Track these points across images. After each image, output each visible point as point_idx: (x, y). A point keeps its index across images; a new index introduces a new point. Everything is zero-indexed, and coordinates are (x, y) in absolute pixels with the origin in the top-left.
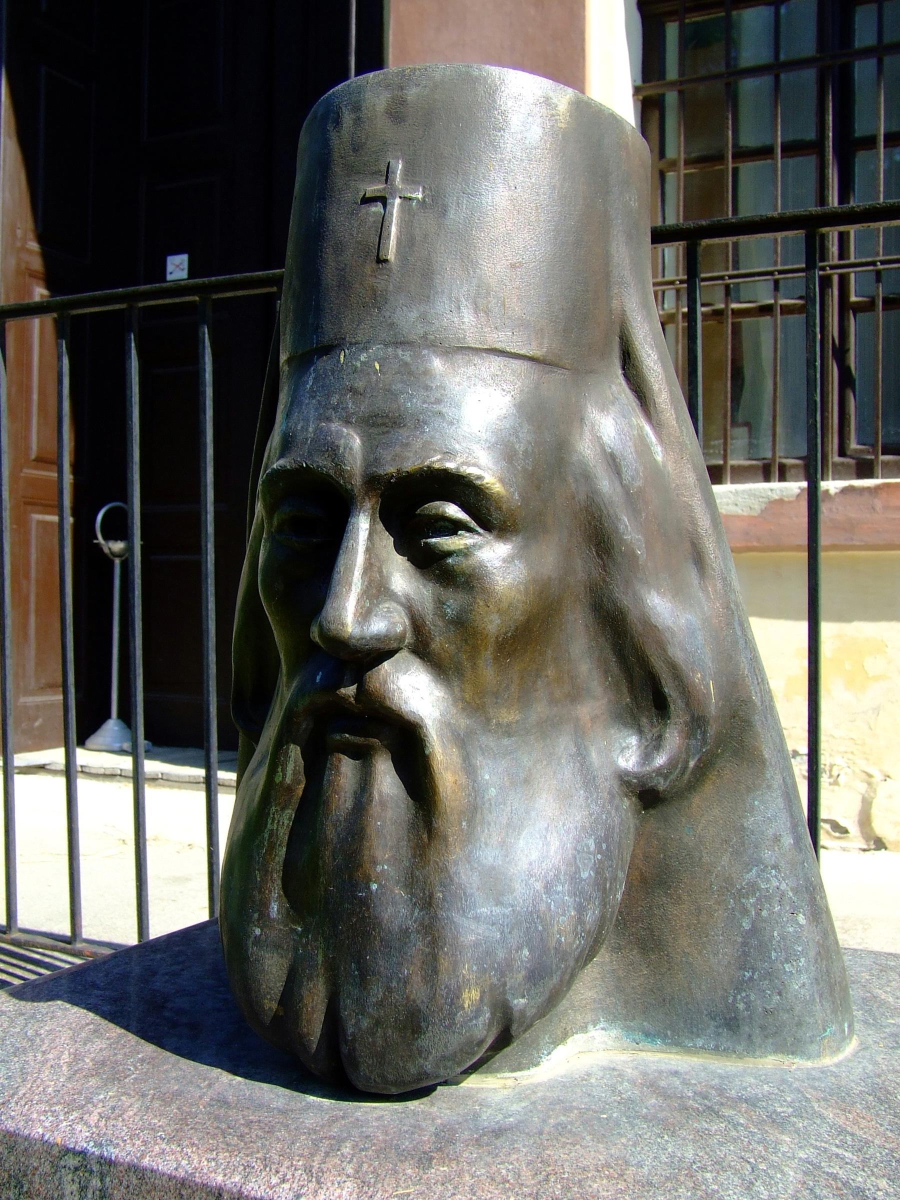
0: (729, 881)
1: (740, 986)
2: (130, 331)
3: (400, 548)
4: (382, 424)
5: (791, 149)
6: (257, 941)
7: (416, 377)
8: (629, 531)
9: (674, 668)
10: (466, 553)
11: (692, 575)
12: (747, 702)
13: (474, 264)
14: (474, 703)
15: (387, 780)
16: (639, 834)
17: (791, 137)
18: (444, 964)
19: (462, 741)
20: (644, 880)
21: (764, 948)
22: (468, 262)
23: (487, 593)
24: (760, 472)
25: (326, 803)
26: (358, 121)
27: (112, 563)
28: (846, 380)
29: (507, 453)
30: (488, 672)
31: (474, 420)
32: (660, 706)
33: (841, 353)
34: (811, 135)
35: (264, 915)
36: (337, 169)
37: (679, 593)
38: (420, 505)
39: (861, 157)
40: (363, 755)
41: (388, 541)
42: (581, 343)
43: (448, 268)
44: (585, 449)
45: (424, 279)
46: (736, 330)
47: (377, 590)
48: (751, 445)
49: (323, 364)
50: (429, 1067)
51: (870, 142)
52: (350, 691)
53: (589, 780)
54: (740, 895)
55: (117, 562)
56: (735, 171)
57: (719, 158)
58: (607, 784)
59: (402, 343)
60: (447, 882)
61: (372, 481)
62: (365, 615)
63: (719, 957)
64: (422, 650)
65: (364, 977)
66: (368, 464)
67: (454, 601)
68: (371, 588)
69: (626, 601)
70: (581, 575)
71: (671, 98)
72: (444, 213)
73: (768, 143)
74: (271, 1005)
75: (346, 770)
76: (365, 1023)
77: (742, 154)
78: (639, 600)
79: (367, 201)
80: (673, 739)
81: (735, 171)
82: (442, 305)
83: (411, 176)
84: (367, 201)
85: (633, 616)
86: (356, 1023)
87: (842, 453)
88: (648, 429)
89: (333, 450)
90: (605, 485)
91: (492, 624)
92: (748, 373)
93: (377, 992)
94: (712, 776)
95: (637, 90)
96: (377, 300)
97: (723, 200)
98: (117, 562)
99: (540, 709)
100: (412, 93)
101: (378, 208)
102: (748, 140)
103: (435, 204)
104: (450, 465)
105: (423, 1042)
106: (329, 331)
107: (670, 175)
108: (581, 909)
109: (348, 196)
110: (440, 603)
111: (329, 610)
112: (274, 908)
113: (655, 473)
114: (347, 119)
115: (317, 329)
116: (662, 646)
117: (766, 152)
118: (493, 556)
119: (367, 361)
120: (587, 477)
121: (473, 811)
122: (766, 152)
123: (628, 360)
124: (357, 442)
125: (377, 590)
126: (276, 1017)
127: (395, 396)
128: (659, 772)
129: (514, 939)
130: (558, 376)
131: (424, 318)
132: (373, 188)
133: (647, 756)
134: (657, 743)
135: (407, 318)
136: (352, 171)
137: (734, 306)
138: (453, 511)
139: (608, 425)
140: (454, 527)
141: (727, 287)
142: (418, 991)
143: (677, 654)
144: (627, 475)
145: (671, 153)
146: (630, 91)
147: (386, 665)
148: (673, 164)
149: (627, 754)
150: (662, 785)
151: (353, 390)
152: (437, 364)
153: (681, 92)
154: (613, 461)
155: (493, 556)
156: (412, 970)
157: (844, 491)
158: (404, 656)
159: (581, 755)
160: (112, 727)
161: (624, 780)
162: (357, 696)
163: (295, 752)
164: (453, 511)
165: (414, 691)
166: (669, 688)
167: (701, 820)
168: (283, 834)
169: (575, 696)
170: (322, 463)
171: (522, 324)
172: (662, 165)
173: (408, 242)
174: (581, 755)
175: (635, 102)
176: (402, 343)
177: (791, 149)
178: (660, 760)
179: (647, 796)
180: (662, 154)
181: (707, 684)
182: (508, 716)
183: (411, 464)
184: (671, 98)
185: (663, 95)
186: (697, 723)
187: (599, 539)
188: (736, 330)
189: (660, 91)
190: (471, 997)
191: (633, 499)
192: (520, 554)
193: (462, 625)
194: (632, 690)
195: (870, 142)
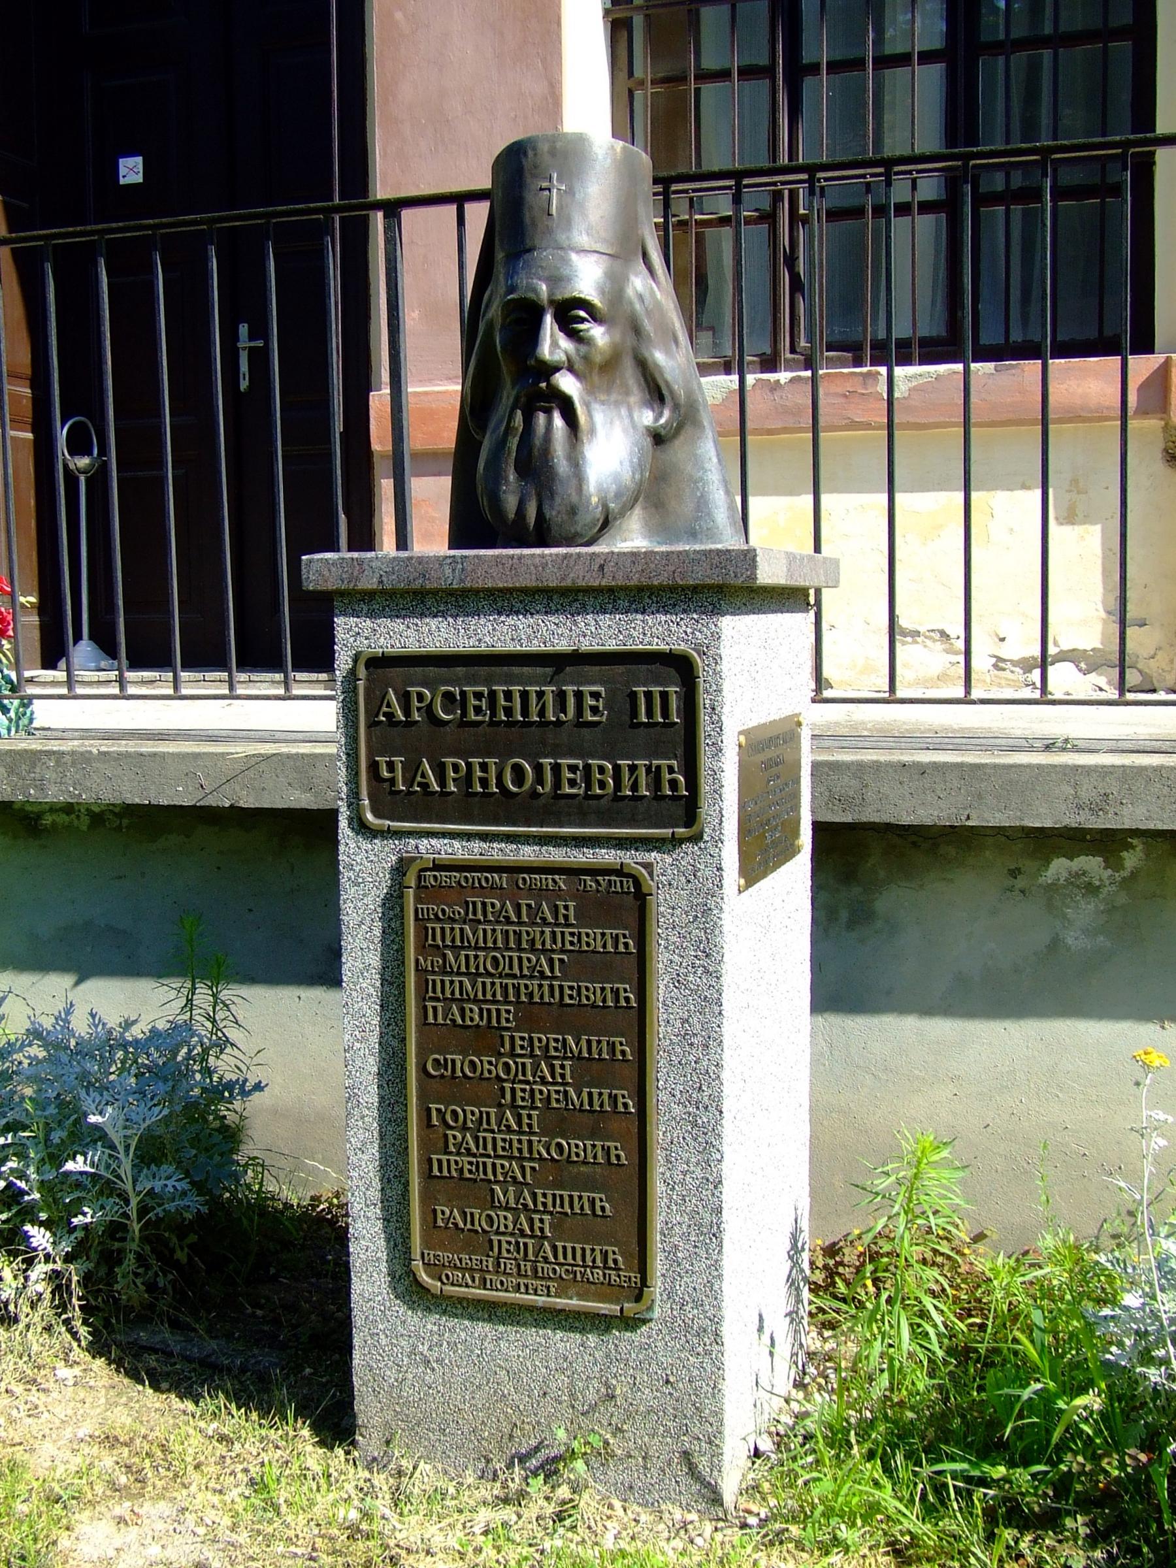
0: (691, 476)
1: (698, 519)
2: (268, 240)
3: (561, 330)
4: (555, 280)
5: (747, 73)
6: (505, 492)
7: (566, 261)
8: (648, 326)
9: (667, 382)
10: (587, 330)
11: (674, 347)
12: (696, 401)
13: (587, 216)
14: (591, 390)
15: (558, 421)
16: (653, 458)
17: (747, 62)
18: (585, 487)
19: (587, 405)
20: (656, 478)
21: (706, 503)
22: (585, 216)
23: (595, 345)
24: (722, 368)
25: (534, 431)
26: (535, 155)
27: (77, 479)
28: (796, 285)
29: (602, 292)
30: (596, 378)
31: (587, 278)
32: (661, 399)
33: (791, 261)
34: (764, 61)
35: (507, 480)
36: (527, 174)
37: (668, 352)
38: (570, 312)
39: (808, 82)
40: (548, 411)
41: (556, 327)
42: (625, 251)
43: (576, 218)
44: (630, 292)
45: (568, 223)
46: (700, 239)
47: (555, 344)
48: (715, 344)
49: (526, 256)
50: (579, 529)
51: (814, 69)
52: (543, 385)
53: (634, 427)
54: (696, 482)
55: (82, 478)
56: (698, 91)
57: (683, 79)
58: (642, 430)
59: (562, 248)
60: (584, 458)
61: (552, 302)
62: (551, 353)
63: (688, 508)
64: (571, 369)
65: (552, 497)
66: (549, 296)
67: (583, 349)
68: (553, 344)
69: (647, 355)
70: (629, 344)
71: (638, 21)
72: (574, 195)
73: (727, 66)
74: (511, 516)
75: (541, 418)
76: (554, 513)
77: (704, 76)
78: (652, 355)
79: (541, 189)
80: (667, 414)
81: (698, 91)
82: (575, 233)
83: (560, 180)
84: (541, 189)
85: (650, 360)
86: (549, 513)
87: (793, 350)
88: (654, 285)
89: (535, 290)
90: (638, 306)
91: (598, 359)
92: (711, 282)
93: (558, 500)
94: (683, 432)
95: (607, 13)
96: (549, 231)
97: (686, 119)
98: (82, 478)
99: (614, 397)
100: (559, 145)
101: (547, 193)
102: (710, 62)
103: (570, 192)
104: (582, 296)
105: (577, 518)
106: (529, 244)
107: (638, 93)
108: (634, 474)
109: (533, 187)
110: (577, 350)
111: (539, 350)
112: (511, 477)
113: (658, 304)
114: (530, 153)
115: (523, 242)
116: (662, 375)
117: (724, 75)
118: (598, 333)
119: (545, 256)
120: (631, 303)
121: (592, 431)
122: (724, 75)
123: (645, 255)
124: (544, 287)
125: (555, 344)
126: (514, 520)
127: (559, 269)
128: (661, 426)
129: (609, 480)
130: (619, 262)
131: (568, 238)
132: (545, 185)
133: (656, 420)
134: (661, 415)
135: (561, 237)
136: (535, 176)
137: (697, 217)
138: (582, 314)
139: (638, 283)
140: (583, 320)
141: (691, 199)
142: (574, 498)
143: (669, 377)
144: (647, 302)
145: (638, 73)
146: (600, 14)
147: (557, 375)
148: (642, 83)
149: (647, 417)
150: (663, 432)
151: (542, 267)
152: (574, 257)
153: (646, 16)
154: (641, 297)
155: (598, 333)
156: (572, 492)
157: (792, 380)
158: (563, 371)
159: (631, 416)
160: (83, 651)
161: (648, 429)
162: (547, 387)
163: (519, 412)
164: (582, 314)
165: (567, 383)
166: (665, 392)
167: (677, 450)
168: (514, 447)
169: (627, 393)
170: (531, 295)
171: (605, 241)
172: (630, 84)
173: (560, 208)
174: (631, 416)
175: (605, 23)
176: (562, 248)
177: (747, 73)
178: (662, 421)
179: (658, 438)
180: (631, 74)
181: (681, 393)
182: (603, 397)
183: (567, 296)
184: (638, 21)
185: (632, 18)
186: (676, 407)
187: (636, 329)
188: (700, 239)
189: (628, 14)
190: (594, 500)
191: (648, 313)
192: (608, 331)
193: (586, 359)
194: (650, 393)
195: (814, 69)
